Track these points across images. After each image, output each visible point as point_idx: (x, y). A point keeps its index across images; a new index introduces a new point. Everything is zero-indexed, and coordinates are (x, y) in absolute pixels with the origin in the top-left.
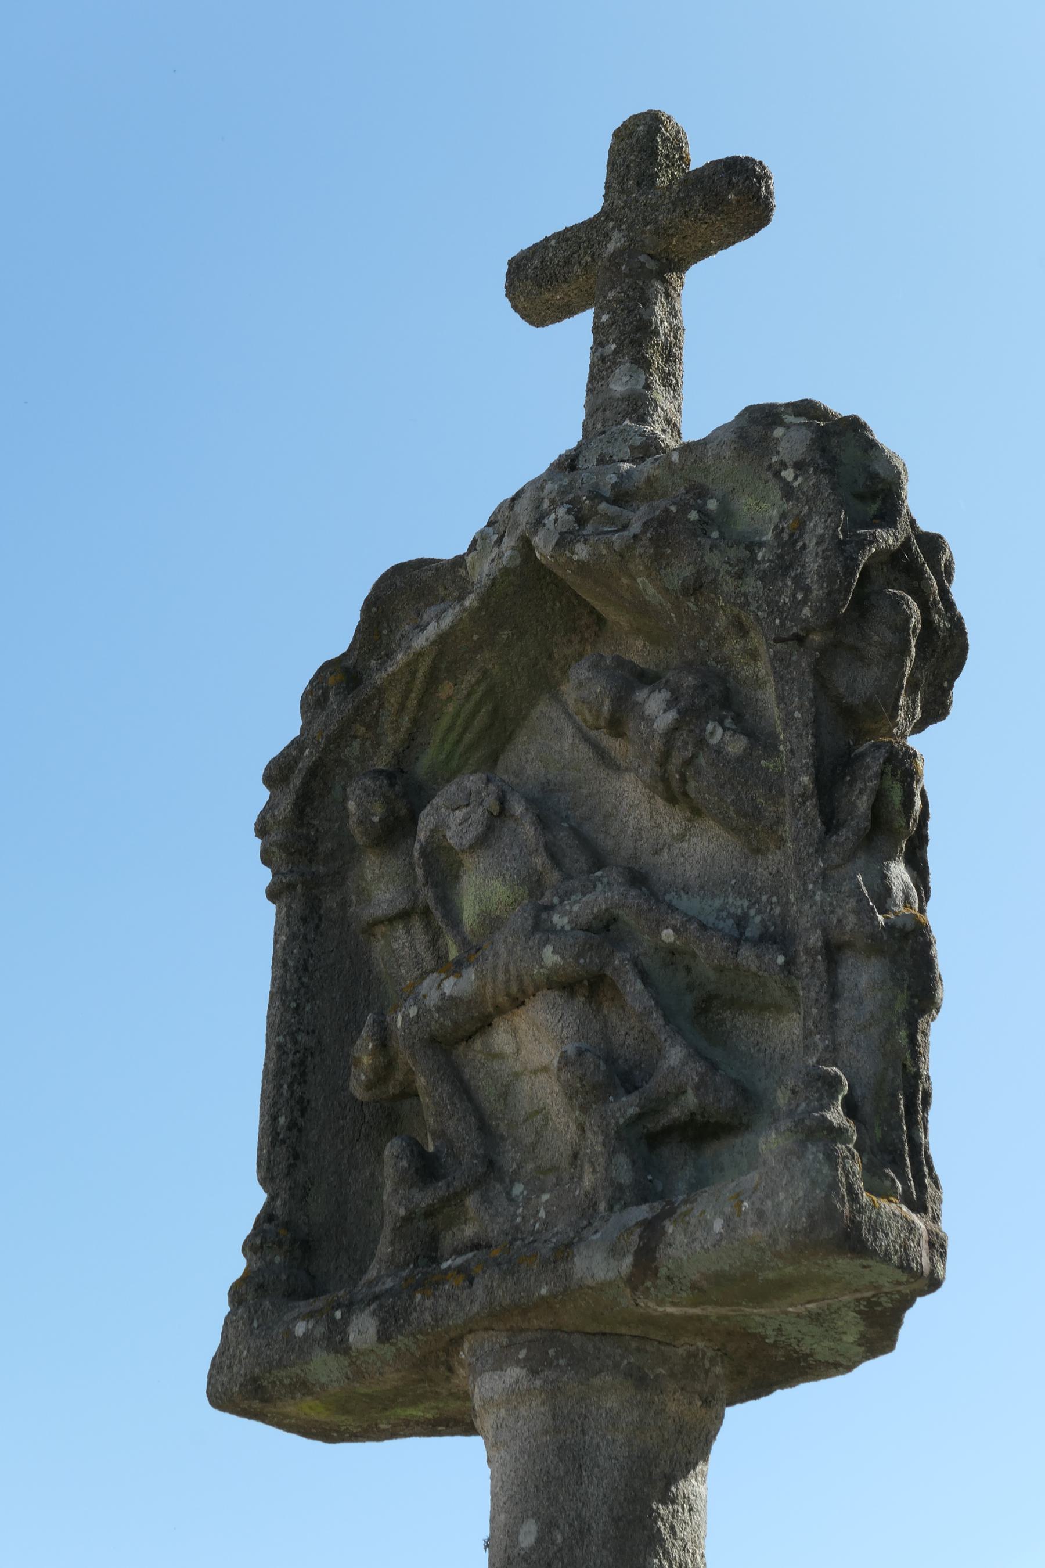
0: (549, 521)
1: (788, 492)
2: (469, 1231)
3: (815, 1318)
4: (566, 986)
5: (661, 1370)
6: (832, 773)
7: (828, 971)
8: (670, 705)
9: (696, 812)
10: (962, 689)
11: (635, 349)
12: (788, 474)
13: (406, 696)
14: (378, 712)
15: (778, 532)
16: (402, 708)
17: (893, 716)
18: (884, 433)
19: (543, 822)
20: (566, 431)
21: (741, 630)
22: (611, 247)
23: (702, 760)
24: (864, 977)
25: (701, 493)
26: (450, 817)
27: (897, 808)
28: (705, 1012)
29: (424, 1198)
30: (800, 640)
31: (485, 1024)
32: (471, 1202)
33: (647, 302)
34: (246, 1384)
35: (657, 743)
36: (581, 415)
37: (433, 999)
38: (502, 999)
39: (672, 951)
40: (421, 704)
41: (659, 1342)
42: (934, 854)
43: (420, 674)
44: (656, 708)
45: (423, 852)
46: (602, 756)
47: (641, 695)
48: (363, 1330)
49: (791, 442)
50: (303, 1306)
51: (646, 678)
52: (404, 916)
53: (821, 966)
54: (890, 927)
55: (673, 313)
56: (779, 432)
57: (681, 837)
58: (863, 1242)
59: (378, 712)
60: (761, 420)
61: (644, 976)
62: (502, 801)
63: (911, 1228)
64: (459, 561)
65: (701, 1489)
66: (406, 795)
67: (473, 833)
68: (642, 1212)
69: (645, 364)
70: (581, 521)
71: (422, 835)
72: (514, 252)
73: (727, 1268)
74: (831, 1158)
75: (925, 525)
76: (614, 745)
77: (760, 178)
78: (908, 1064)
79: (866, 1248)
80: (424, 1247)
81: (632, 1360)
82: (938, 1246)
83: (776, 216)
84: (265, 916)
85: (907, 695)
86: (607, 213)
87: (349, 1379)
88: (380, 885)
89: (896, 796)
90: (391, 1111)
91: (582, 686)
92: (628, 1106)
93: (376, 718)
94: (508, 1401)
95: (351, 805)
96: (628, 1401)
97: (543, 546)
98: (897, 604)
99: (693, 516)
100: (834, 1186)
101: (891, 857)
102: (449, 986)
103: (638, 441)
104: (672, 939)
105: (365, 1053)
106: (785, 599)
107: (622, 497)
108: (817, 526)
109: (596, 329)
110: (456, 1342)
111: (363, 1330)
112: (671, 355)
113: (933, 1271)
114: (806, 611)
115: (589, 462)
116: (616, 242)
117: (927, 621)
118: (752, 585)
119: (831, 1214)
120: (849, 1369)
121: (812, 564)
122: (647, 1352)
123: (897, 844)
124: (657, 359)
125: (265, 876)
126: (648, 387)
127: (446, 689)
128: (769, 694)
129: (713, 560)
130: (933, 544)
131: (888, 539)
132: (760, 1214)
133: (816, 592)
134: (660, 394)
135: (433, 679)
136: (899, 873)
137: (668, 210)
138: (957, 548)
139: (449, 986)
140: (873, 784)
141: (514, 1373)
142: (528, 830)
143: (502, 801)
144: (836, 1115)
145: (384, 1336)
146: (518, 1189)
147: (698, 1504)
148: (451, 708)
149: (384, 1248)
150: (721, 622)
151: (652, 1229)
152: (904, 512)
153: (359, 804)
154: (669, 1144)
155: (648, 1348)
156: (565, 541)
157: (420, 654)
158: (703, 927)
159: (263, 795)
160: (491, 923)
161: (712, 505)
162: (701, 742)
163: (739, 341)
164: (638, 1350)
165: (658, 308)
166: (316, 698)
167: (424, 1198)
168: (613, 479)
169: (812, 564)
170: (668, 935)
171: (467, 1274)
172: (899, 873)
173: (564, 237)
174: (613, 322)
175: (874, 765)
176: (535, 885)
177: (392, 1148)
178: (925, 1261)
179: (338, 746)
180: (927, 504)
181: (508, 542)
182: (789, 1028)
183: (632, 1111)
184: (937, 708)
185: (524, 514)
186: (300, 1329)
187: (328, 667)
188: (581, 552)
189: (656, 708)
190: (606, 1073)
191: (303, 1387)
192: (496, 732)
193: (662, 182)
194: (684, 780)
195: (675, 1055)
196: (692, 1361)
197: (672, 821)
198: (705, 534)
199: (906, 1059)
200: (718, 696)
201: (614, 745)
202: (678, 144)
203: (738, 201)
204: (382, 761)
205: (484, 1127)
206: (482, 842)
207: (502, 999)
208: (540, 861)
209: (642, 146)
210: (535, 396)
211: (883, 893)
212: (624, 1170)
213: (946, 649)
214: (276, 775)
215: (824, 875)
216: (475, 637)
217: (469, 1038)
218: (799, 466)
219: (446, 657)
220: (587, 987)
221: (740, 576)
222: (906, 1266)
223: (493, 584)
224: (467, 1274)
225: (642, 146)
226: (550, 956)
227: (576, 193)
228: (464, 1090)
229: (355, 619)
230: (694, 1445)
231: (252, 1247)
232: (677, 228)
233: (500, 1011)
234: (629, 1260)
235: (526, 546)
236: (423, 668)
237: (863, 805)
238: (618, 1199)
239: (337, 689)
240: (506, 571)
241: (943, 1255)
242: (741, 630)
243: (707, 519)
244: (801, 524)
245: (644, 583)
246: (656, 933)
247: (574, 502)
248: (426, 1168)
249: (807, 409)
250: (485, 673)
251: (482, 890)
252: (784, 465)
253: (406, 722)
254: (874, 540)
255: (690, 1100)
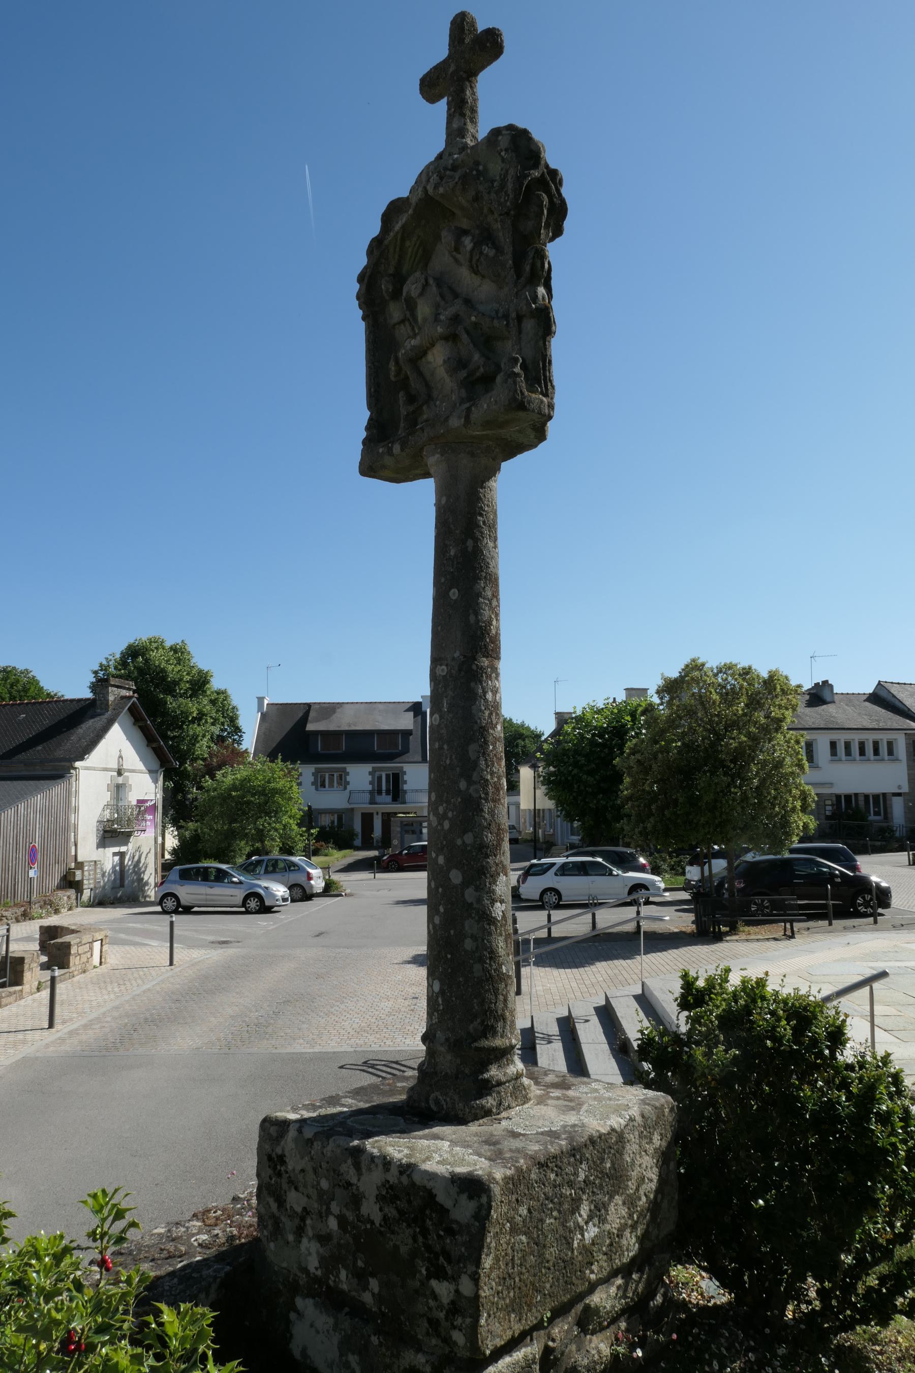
0: (431, 180)
1: (503, 160)
2: (425, 417)
3: (520, 431)
4: (446, 338)
6: (519, 259)
8: (472, 241)
9: (483, 277)
10: (567, 224)
11: (461, 111)
12: (503, 153)
15: (501, 175)
17: (539, 237)
18: (536, 135)
19: (439, 286)
20: (439, 144)
21: (492, 212)
22: (451, 70)
23: (482, 259)
24: (529, 325)
25: (477, 163)
26: (412, 288)
28: (486, 342)
29: (411, 408)
30: (507, 214)
31: (424, 353)
32: (425, 408)
33: (463, 91)
34: (371, 467)
35: (468, 255)
36: (445, 137)
37: (408, 347)
38: (428, 345)
39: (476, 324)
42: (554, 283)
44: (468, 243)
45: (405, 300)
46: (457, 261)
47: (463, 239)
48: (397, 449)
49: (504, 142)
50: (382, 444)
51: (465, 232)
52: (402, 321)
53: (516, 323)
54: (537, 308)
55: (474, 93)
56: (500, 138)
57: (480, 286)
58: (525, 407)
60: (496, 133)
61: (468, 333)
62: (426, 280)
63: (542, 402)
64: (408, 198)
65: (494, 484)
66: (399, 280)
67: (419, 291)
68: (467, 405)
69: (463, 115)
70: (441, 178)
71: (404, 294)
72: (421, 76)
74: (515, 383)
75: (552, 166)
76: (458, 256)
77: (498, 36)
80: (413, 421)
82: (551, 406)
83: (505, 50)
84: (362, 325)
85: (545, 228)
86: (449, 56)
88: (395, 312)
89: (539, 264)
90: (404, 383)
91: (447, 237)
92: (463, 374)
95: (383, 287)
97: (430, 188)
98: (539, 196)
99: (474, 173)
100: (516, 390)
101: (538, 285)
102: (413, 342)
103: (461, 146)
105: (392, 367)
106: (502, 200)
107: (454, 168)
108: (512, 172)
109: (448, 103)
110: (422, 449)
111: (397, 449)
112: (474, 111)
113: (549, 414)
114: (508, 204)
115: (445, 157)
116: (452, 68)
117: (551, 201)
118: (493, 196)
119: (515, 399)
120: (536, 446)
121: (510, 185)
123: (540, 280)
124: (468, 113)
125: (361, 313)
126: (465, 124)
127: (408, 243)
128: (501, 234)
129: (481, 188)
130: (554, 173)
131: (536, 174)
132: (496, 401)
133: (511, 196)
134: (470, 126)
135: (403, 240)
136: (541, 290)
137: (473, 48)
138: (564, 173)
139: (413, 342)
140: (530, 261)
141: (437, 456)
142: (434, 289)
143: (426, 280)
144: (517, 369)
145: (402, 450)
146: (438, 403)
147: (493, 489)
148: (410, 250)
149: (402, 425)
150: (485, 210)
151: (469, 410)
152: (543, 162)
153: (385, 286)
154: (477, 384)
156: (436, 187)
157: (397, 232)
158: (483, 315)
159: (358, 286)
160: (425, 320)
161: (481, 168)
162: (481, 253)
163: (498, 101)
165: (468, 92)
166: (370, 252)
167: (411, 408)
168: (451, 161)
169: (510, 185)
170: (473, 318)
171: (422, 429)
172: (541, 290)
173: (435, 68)
174: (453, 100)
175: (531, 254)
176: (437, 306)
177: (401, 394)
178: (547, 411)
180: (552, 158)
181: (420, 189)
182: (509, 344)
183: (465, 375)
184: (558, 232)
185: (424, 179)
186: (381, 450)
187: (373, 240)
188: (441, 190)
189: (468, 243)
190: (458, 364)
191: (384, 467)
192: (426, 256)
193: (467, 41)
194: (477, 266)
195: (476, 357)
197: (477, 280)
198: (479, 179)
200: (486, 237)
201: (458, 256)
202: (473, 24)
204: (391, 270)
205: (427, 385)
206: (421, 294)
207: (428, 345)
208: (438, 299)
209: (461, 25)
210: (423, 134)
211: (535, 298)
212: (463, 393)
213: (559, 212)
214: (361, 279)
215: (517, 293)
217: (421, 358)
218: (506, 150)
219: (406, 232)
220: (451, 338)
221: (489, 193)
222: (540, 413)
224: (422, 429)
225: (461, 25)
226: (439, 330)
227: (438, 50)
228: (420, 374)
229: (380, 224)
230: (493, 470)
231: (367, 428)
233: (428, 349)
234: (463, 420)
235: (425, 190)
236: (399, 237)
237: (528, 268)
238: (462, 402)
239: (377, 247)
240: (420, 200)
241: (553, 409)
242: (492, 212)
243: (479, 173)
244: (507, 171)
246: (470, 319)
247: (439, 172)
248: (411, 399)
249: (511, 127)
250: (419, 236)
251: (424, 310)
252: (502, 150)
253: (397, 257)
254: (530, 175)
255: (482, 370)
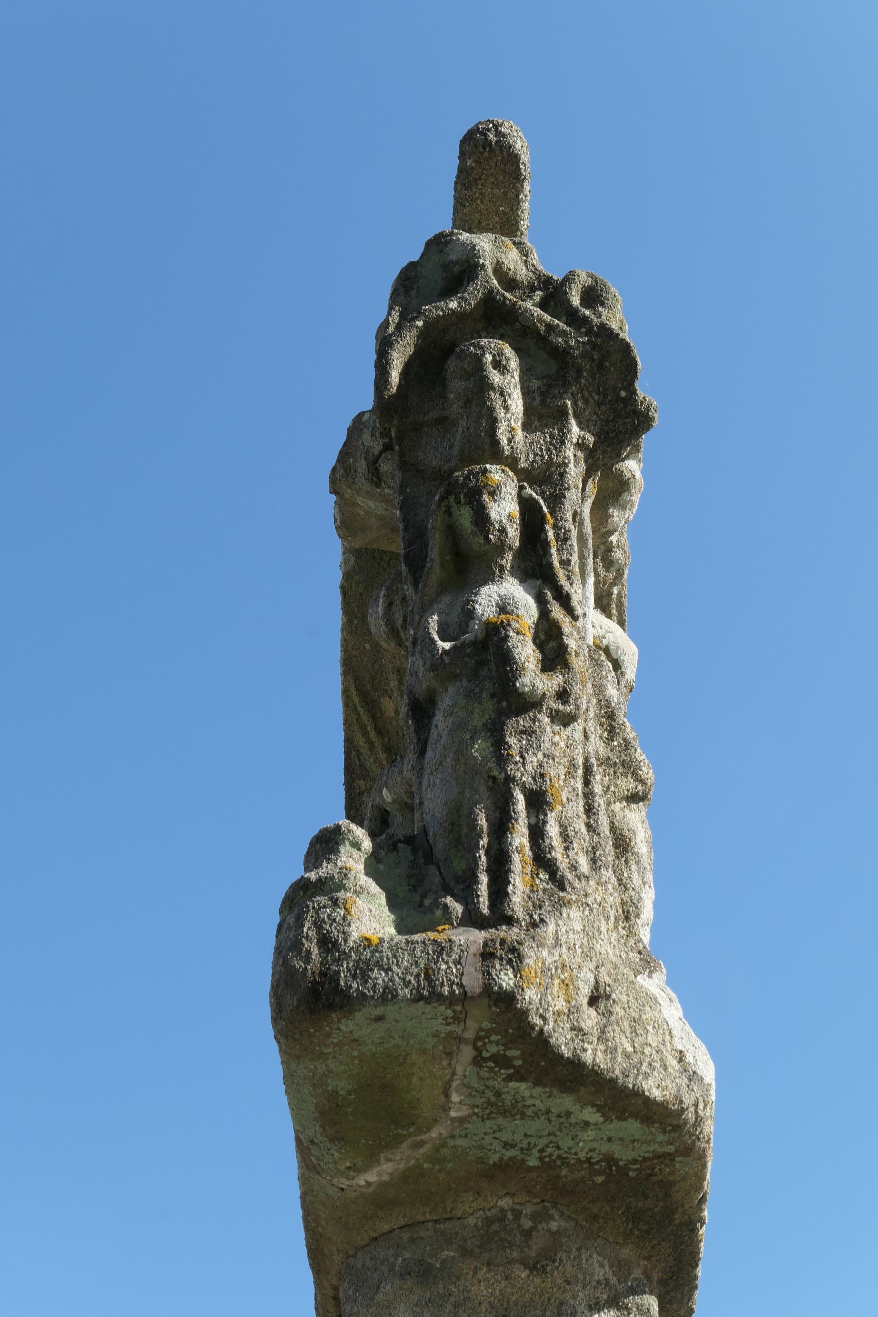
5: (446, 1252)
7: (417, 731)
13: (366, 734)
14: (360, 761)
27: (469, 531)
40: (380, 732)
41: (436, 1222)
59: (360, 761)
78: (495, 773)
79: (349, 997)
81: (407, 1255)
89: (464, 517)
96: (417, 1305)
122: (423, 1238)
155: (422, 1233)
164: (412, 1241)
179: (357, 810)
184: (361, 415)
196: (495, 1227)
199: (490, 769)
203: (475, 161)
216: (368, 646)
232: (467, 221)
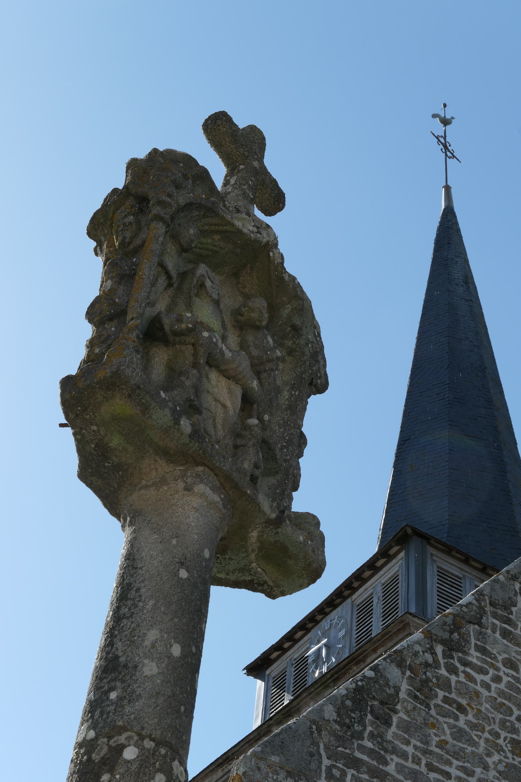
16: (211, 225)
43: (225, 228)
73: (291, 549)
87: (161, 427)
93: (208, 217)
94: (211, 504)
104: (266, 419)
127: (217, 237)
157: (233, 225)
216: (239, 242)
223: (258, 242)
245: (289, 307)
